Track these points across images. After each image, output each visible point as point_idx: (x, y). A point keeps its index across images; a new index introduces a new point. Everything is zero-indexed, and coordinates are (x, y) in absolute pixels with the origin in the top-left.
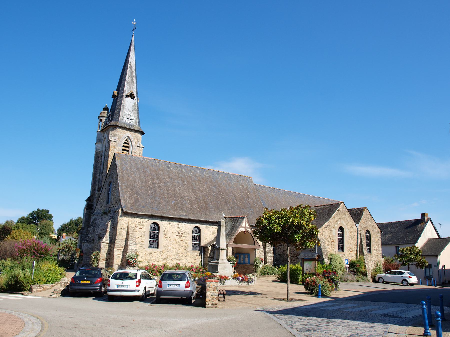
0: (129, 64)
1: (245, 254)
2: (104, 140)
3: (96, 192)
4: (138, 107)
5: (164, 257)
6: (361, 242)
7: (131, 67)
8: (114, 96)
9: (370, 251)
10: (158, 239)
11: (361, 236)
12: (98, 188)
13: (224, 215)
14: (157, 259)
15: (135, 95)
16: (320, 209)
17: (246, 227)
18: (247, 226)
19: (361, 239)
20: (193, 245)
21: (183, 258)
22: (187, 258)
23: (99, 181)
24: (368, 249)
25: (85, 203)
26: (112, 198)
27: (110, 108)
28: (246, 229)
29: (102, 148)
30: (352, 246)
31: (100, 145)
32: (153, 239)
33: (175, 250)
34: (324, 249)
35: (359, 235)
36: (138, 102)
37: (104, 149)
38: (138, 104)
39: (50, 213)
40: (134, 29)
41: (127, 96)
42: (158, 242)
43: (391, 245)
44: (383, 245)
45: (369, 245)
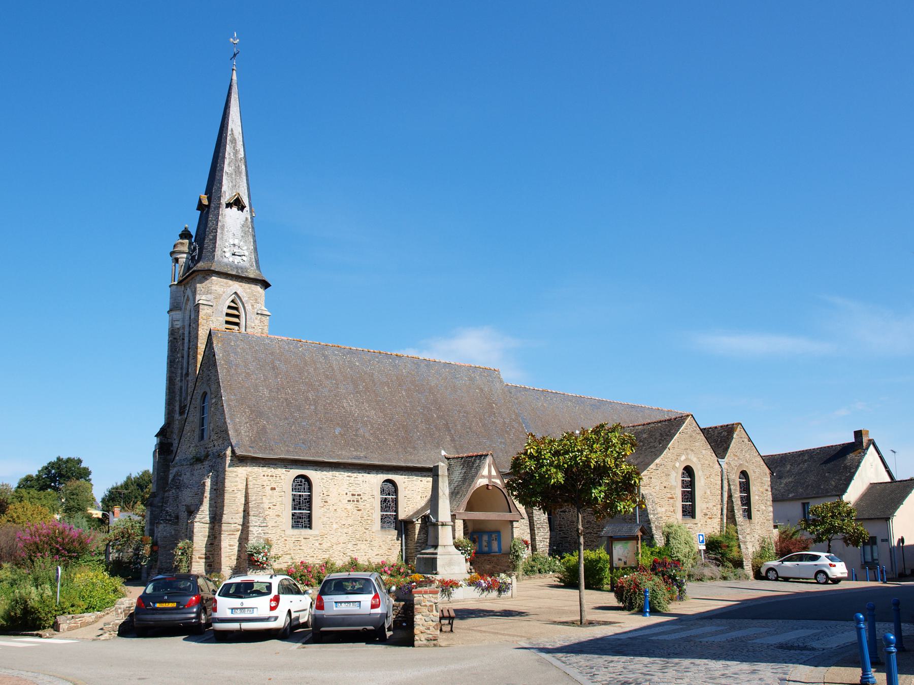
0: (229, 133)
1: (490, 533)
2: (186, 304)
3: (177, 416)
4: (253, 228)
5: (325, 546)
6: (730, 496)
7: (234, 141)
8: (201, 206)
9: (748, 514)
10: (310, 508)
11: (729, 485)
12: (181, 408)
13: (443, 453)
14: (310, 551)
15: (246, 201)
16: (643, 431)
17: (490, 476)
18: (494, 473)
19: (730, 490)
20: (383, 519)
21: (363, 546)
22: (371, 546)
23: (181, 393)
24: (744, 511)
25: (155, 441)
26: (209, 427)
27: (193, 233)
28: (490, 481)
29: (183, 321)
30: (710, 505)
31: (177, 315)
32: (300, 509)
33: (345, 531)
34: (654, 514)
35: (725, 482)
36: (252, 218)
37: (187, 323)
38: (252, 222)
39: (83, 465)
40: (235, 55)
41: (229, 205)
42: (310, 517)
43: (792, 499)
44: (775, 500)
45: (747, 501)
